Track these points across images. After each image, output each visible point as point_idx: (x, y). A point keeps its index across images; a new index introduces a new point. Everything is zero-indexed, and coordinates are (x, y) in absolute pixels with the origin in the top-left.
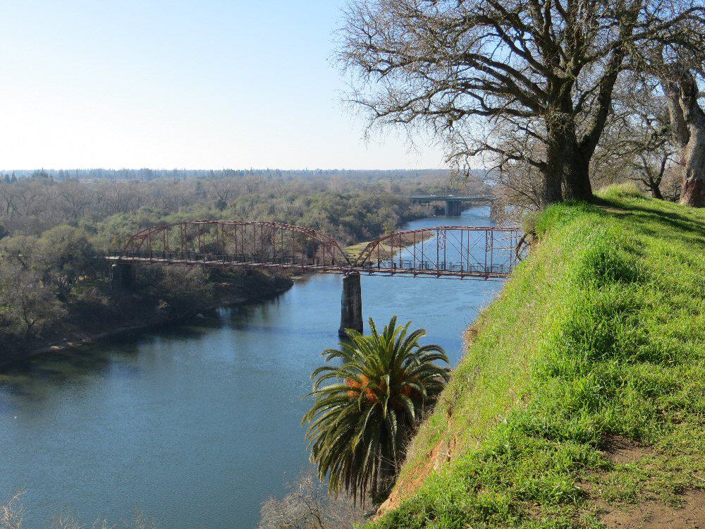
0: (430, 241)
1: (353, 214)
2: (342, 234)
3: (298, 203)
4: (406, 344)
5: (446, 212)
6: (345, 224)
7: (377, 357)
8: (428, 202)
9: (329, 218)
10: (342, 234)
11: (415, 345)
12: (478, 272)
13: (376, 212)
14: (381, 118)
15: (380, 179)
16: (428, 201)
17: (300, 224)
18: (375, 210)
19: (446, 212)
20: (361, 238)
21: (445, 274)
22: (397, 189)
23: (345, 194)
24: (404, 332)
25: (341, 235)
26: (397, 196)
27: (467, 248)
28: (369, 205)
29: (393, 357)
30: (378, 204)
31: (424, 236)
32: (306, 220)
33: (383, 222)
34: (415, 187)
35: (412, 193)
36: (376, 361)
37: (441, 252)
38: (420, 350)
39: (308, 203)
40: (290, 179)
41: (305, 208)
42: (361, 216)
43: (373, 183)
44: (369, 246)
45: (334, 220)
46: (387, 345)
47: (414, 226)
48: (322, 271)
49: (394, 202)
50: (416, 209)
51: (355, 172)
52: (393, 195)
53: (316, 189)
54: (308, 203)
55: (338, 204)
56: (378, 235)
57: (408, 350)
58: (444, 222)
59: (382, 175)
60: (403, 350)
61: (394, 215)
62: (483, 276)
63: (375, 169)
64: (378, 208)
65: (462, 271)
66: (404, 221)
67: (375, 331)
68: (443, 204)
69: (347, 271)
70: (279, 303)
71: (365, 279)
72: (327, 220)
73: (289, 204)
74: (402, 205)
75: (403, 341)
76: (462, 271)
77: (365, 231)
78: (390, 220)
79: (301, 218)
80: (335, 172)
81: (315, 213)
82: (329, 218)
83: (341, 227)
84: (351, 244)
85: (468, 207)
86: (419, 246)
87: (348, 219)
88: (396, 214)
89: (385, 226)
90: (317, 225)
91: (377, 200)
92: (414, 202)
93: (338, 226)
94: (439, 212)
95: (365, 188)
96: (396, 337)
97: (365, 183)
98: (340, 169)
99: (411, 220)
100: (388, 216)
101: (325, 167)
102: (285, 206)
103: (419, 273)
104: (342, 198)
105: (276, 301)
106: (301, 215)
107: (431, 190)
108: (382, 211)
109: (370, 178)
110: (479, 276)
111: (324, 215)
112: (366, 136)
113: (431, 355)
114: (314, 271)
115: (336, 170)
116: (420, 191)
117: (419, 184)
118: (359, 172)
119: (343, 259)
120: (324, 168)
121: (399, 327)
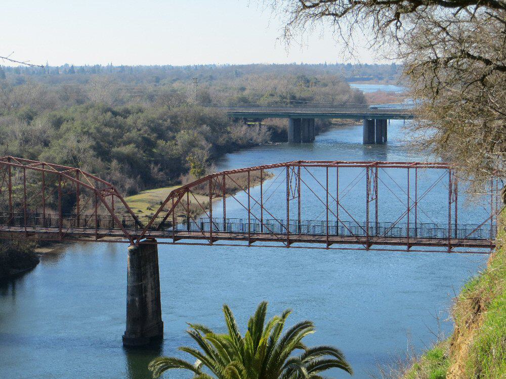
0: (275, 183)
1: (135, 142)
2: (117, 175)
3: (40, 124)
4: (282, 346)
5: (290, 136)
6: (122, 158)
7: (241, 367)
8: (260, 120)
9: (94, 148)
10: (117, 175)
11: (299, 346)
12: (357, 237)
13: (174, 138)
14: (307, 10)
15: (175, 80)
16: (258, 118)
17: (47, 159)
18: (171, 134)
19: (290, 136)
20: (150, 183)
21: (467, 246)
22: (206, 99)
23: (118, 108)
24: (279, 327)
25: (114, 178)
26: (207, 111)
27: (335, 197)
28: (160, 125)
29: (264, 368)
30: (175, 124)
31: (259, 174)
32: (56, 153)
33: (186, 153)
34: (236, 95)
35: (231, 105)
36: (240, 372)
37: (293, 203)
38: (306, 355)
39: (58, 123)
40: (20, 82)
41: (51, 132)
42: (147, 144)
43: (164, 88)
44: (172, 195)
45: (103, 153)
46: (255, 348)
47: (237, 162)
48: (94, 238)
49: (201, 120)
50: (240, 131)
51: (131, 69)
52: (199, 108)
53: (66, 99)
54: (58, 123)
55: (107, 125)
56: (178, 175)
57: (287, 355)
58: (291, 155)
59: (177, 74)
60: (277, 354)
61: (204, 143)
62: (363, 243)
63: (166, 64)
64: (177, 131)
65: (408, 237)
66: (220, 152)
67: (233, 326)
68: (284, 123)
69: (135, 237)
70: (14, 294)
71: (166, 251)
72: (92, 152)
73: (25, 126)
74: (217, 126)
75: (278, 341)
76: (289, 234)
77: (156, 169)
78: (196, 150)
79: (46, 149)
80: (96, 70)
81: (71, 142)
82: (94, 148)
83: (114, 163)
84: (132, 192)
85: (326, 127)
86: (255, 190)
87: (127, 150)
88: (207, 140)
89: (190, 160)
90: (74, 160)
91: (174, 118)
92: (236, 120)
93: (110, 161)
94: (278, 137)
95: (151, 98)
96: (265, 339)
97: (150, 88)
98: (104, 64)
99: (230, 152)
100: (192, 144)
101: (80, 60)
102: (18, 127)
103: (296, 241)
104: (115, 114)
105: (10, 291)
106: (46, 144)
107: (263, 101)
108: (183, 136)
109: (158, 80)
110: (356, 243)
111: (87, 143)
112: (286, 33)
113: (322, 362)
114: (68, 239)
115: (98, 66)
116: (244, 101)
117: (243, 89)
118: (139, 69)
119: (129, 221)
120: (78, 63)
121: (272, 319)
